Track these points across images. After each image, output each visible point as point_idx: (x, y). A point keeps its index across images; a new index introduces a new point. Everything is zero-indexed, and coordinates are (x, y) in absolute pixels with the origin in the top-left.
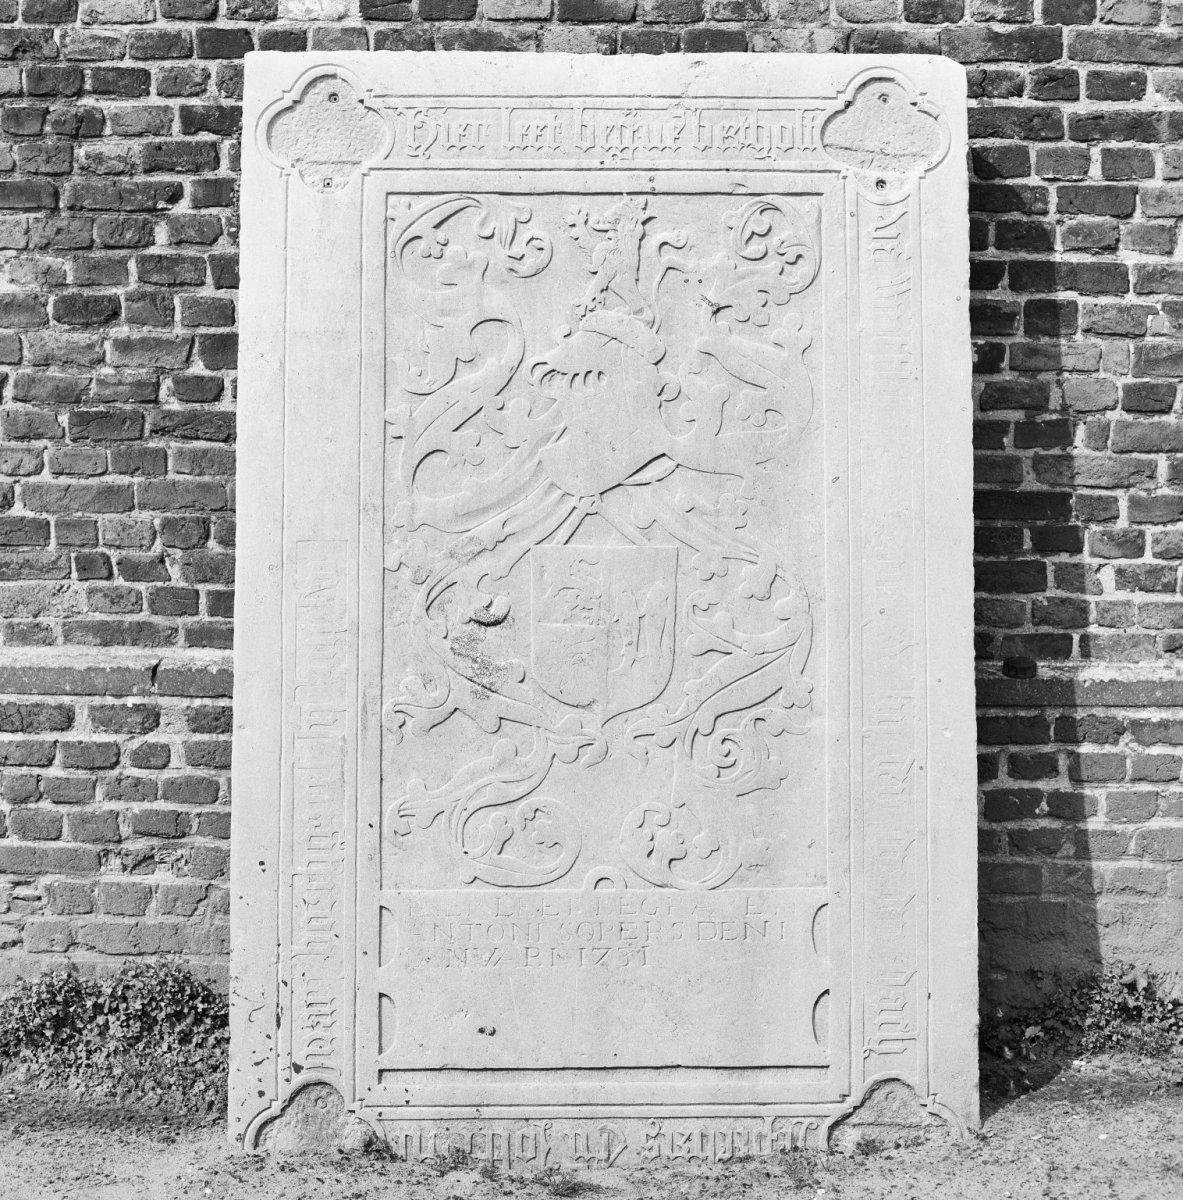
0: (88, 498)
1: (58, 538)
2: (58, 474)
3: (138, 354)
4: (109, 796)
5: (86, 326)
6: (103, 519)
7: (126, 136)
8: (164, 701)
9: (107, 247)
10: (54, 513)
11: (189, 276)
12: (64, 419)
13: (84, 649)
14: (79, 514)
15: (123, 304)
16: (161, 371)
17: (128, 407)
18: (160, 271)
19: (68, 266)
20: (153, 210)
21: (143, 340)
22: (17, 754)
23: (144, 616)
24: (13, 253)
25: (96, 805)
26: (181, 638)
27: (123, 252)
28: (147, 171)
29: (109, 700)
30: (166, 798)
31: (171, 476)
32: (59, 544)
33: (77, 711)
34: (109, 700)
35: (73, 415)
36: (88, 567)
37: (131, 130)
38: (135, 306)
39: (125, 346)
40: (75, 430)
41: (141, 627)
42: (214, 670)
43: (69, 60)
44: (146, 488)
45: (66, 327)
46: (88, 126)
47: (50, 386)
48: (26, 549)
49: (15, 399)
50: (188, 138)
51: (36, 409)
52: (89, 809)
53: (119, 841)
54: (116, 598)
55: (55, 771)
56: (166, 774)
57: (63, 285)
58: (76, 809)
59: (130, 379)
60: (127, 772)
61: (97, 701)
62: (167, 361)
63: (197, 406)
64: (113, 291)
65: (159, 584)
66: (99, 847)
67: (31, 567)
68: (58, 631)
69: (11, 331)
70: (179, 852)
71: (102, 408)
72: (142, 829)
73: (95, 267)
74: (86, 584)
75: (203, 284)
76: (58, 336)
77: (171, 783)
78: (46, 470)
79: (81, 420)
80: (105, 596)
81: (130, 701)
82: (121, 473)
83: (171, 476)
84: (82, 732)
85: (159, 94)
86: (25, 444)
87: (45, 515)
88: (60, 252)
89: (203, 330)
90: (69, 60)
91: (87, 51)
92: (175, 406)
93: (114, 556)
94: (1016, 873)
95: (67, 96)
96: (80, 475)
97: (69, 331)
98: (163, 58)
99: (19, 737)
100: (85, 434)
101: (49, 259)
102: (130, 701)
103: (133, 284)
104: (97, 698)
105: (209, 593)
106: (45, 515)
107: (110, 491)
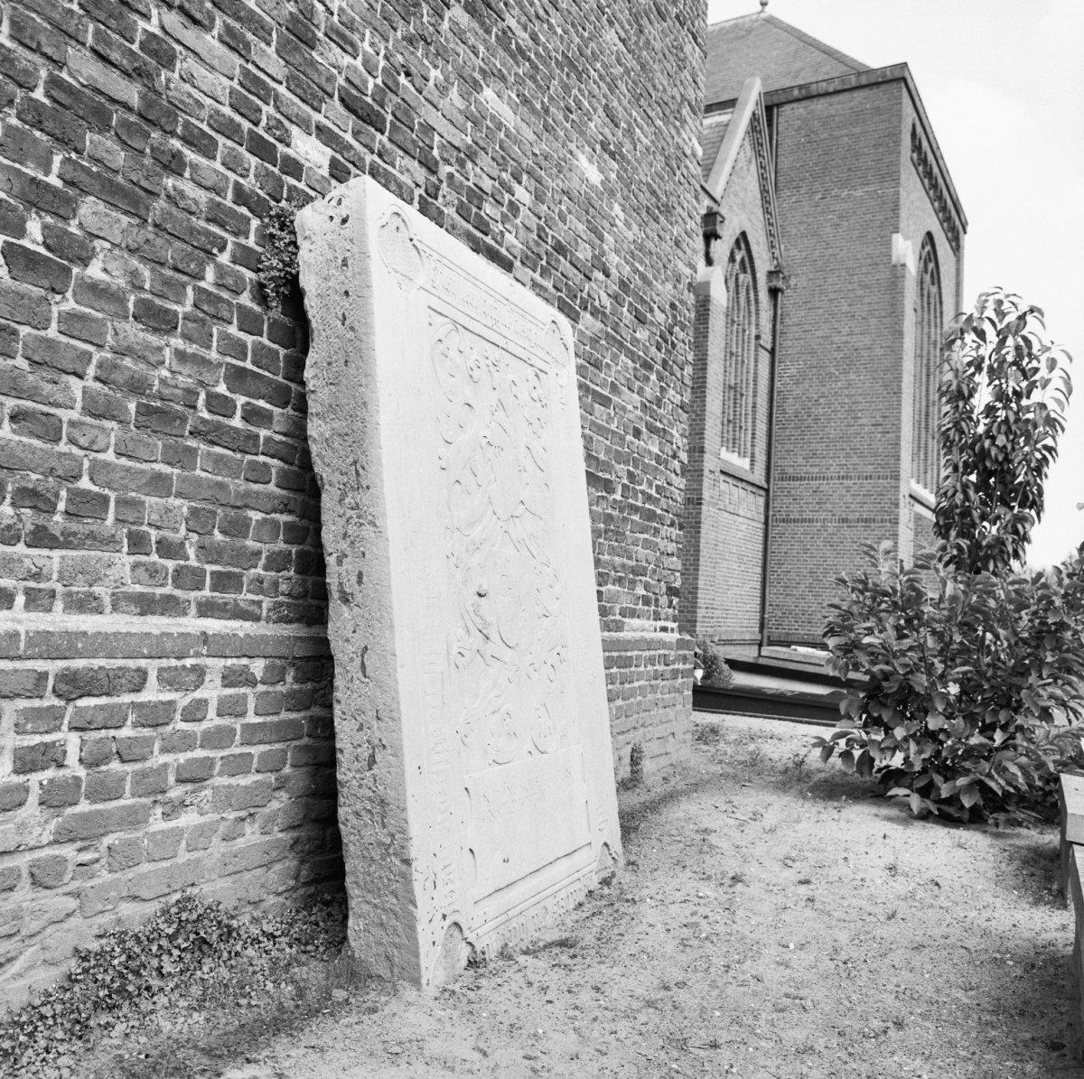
0: (144, 481)
1: (117, 512)
2: (119, 454)
3: (189, 366)
4: (164, 750)
5: (156, 330)
6: (151, 501)
7: (200, 185)
8: (210, 662)
9: (176, 269)
10: (115, 490)
11: (226, 314)
12: (132, 407)
13: (128, 618)
14: (133, 494)
15: (181, 322)
16: (201, 383)
17: (179, 408)
18: (210, 303)
19: (147, 274)
20: (209, 252)
21: (194, 355)
22: (100, 718)
23: (168, 589)
24: (107, 245)
25: (154, 760)
26: (193, 610)
27: (185, 278)
28: (208, 220)
29: (174, 662)
30: (202, 747)
31: (198, 472)
32: (117, 519)
33: (150, 672)
34: (174, 662)
35: (139, 405)
36: (138, 543)
37: (205, 183)
38: (190, 325)
39: (181, 356)
40: (141, 419)
41: (169, 599)
42: (241, 634)
43: (170, 102)
44: (183, 480)
45: (141, 326)
46: (174, 165)
47: (128, 374)
48: (90, 521)
49: (97, 379)
50: (236, 207)
51: (111, 393)
52: (148, 764)
53: (164, 792)
54: (153, 572)
55: (126, 732)
56: (205, 725)
57: (141, 288)
58: (138, 766)
59: (182, 386)
60: (178, 727)
61: (164, 663)
62: (207, 378)
63: (221, 418)
64: (174, 307)
65: (182, 562)
66: (152, 799)
67: (94, 538)
68: (107, 600)
69: (100, 315)
70: (203, 793)
71: (159, 404)
72: (186, 775)
73: (167, 282)
74: (133, 559)
75: (230, 323)
76: (134, 332)
77: (206, 733)
78: (111, 450)
79: (145, 411)
80: (147, 570)
81: (188, 662)
82: (168, 464)
83: (198, 472)
84: (152, 693)
85: (223, 164)
86: (97, 422)
87: (107, 491)
88: (144, 259)
89: (228, 359)
90: (170, 102)
91: (182, 102)
92: (206, 415)
93: (154, 535)
94: (273, 737)
95: (165, 131)
96: (138, 459)
97: (142, 330)
98: (228, 137)
99: (103, 701)
100: (148, 424)
101: (135, 262)
102: (188, 662)
103: (188, 308)
104: (164, 660)
105: (213, 573)
106: (107, 491)
107: (159, 477)
